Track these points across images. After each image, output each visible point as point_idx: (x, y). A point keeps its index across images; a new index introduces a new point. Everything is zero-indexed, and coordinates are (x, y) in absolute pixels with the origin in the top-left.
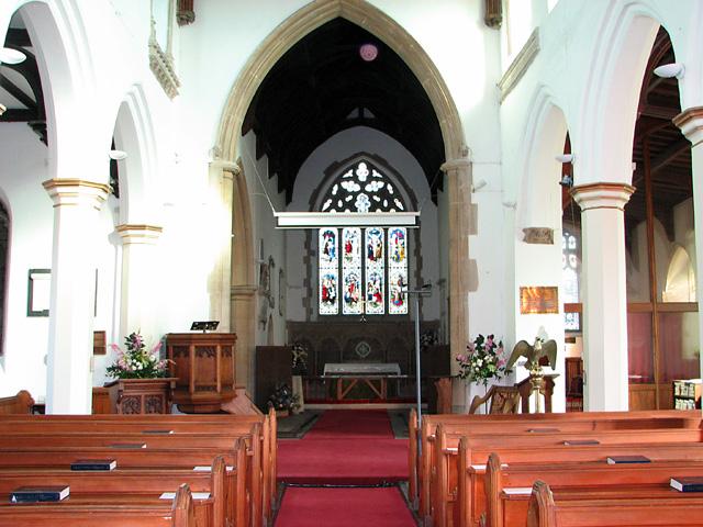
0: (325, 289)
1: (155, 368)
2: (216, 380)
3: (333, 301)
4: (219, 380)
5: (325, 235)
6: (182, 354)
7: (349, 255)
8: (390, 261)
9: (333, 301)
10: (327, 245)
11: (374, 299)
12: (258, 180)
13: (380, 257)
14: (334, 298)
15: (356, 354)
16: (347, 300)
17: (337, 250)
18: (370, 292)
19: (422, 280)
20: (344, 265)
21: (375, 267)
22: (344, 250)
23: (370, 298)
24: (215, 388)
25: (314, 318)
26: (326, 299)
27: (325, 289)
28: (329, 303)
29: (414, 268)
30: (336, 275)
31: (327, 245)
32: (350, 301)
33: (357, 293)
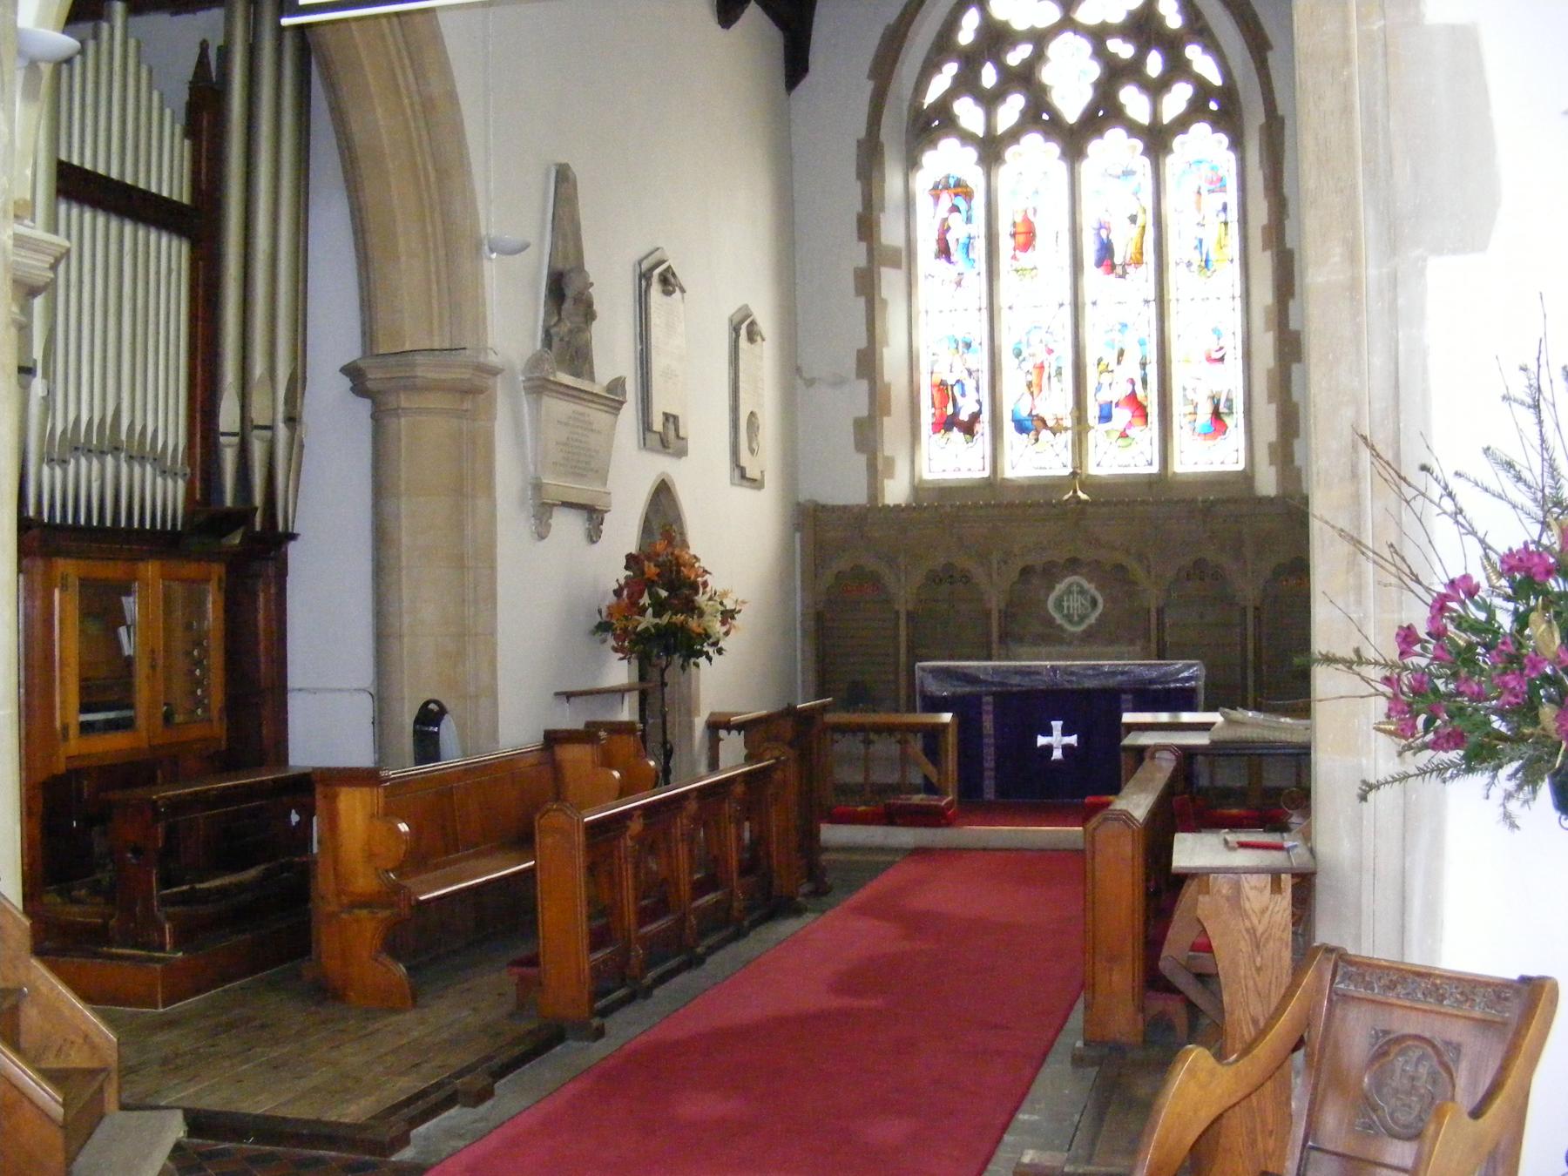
3: (969, 429)
5: (936, 191)
7: (1026, 259)
8: (1174, 275)
9: (969, 429)
10: (944, 230)
11: (1122, 416)
13: (1138, 262)
14: (975, 417)
15: (1050, 622)
16: (1021, 427)
17: (980, 246)
18: (1106, 396)
20: (1003, 299)
21: (1118, 305)
22: (1006, 244)
23: (1106, 417)
25: (896, 492)
26: (946, 423)
28: (956, 435)
29: (1264, 295)
30: (980, 333)
31: (944, 230)
33: (1056, 403)
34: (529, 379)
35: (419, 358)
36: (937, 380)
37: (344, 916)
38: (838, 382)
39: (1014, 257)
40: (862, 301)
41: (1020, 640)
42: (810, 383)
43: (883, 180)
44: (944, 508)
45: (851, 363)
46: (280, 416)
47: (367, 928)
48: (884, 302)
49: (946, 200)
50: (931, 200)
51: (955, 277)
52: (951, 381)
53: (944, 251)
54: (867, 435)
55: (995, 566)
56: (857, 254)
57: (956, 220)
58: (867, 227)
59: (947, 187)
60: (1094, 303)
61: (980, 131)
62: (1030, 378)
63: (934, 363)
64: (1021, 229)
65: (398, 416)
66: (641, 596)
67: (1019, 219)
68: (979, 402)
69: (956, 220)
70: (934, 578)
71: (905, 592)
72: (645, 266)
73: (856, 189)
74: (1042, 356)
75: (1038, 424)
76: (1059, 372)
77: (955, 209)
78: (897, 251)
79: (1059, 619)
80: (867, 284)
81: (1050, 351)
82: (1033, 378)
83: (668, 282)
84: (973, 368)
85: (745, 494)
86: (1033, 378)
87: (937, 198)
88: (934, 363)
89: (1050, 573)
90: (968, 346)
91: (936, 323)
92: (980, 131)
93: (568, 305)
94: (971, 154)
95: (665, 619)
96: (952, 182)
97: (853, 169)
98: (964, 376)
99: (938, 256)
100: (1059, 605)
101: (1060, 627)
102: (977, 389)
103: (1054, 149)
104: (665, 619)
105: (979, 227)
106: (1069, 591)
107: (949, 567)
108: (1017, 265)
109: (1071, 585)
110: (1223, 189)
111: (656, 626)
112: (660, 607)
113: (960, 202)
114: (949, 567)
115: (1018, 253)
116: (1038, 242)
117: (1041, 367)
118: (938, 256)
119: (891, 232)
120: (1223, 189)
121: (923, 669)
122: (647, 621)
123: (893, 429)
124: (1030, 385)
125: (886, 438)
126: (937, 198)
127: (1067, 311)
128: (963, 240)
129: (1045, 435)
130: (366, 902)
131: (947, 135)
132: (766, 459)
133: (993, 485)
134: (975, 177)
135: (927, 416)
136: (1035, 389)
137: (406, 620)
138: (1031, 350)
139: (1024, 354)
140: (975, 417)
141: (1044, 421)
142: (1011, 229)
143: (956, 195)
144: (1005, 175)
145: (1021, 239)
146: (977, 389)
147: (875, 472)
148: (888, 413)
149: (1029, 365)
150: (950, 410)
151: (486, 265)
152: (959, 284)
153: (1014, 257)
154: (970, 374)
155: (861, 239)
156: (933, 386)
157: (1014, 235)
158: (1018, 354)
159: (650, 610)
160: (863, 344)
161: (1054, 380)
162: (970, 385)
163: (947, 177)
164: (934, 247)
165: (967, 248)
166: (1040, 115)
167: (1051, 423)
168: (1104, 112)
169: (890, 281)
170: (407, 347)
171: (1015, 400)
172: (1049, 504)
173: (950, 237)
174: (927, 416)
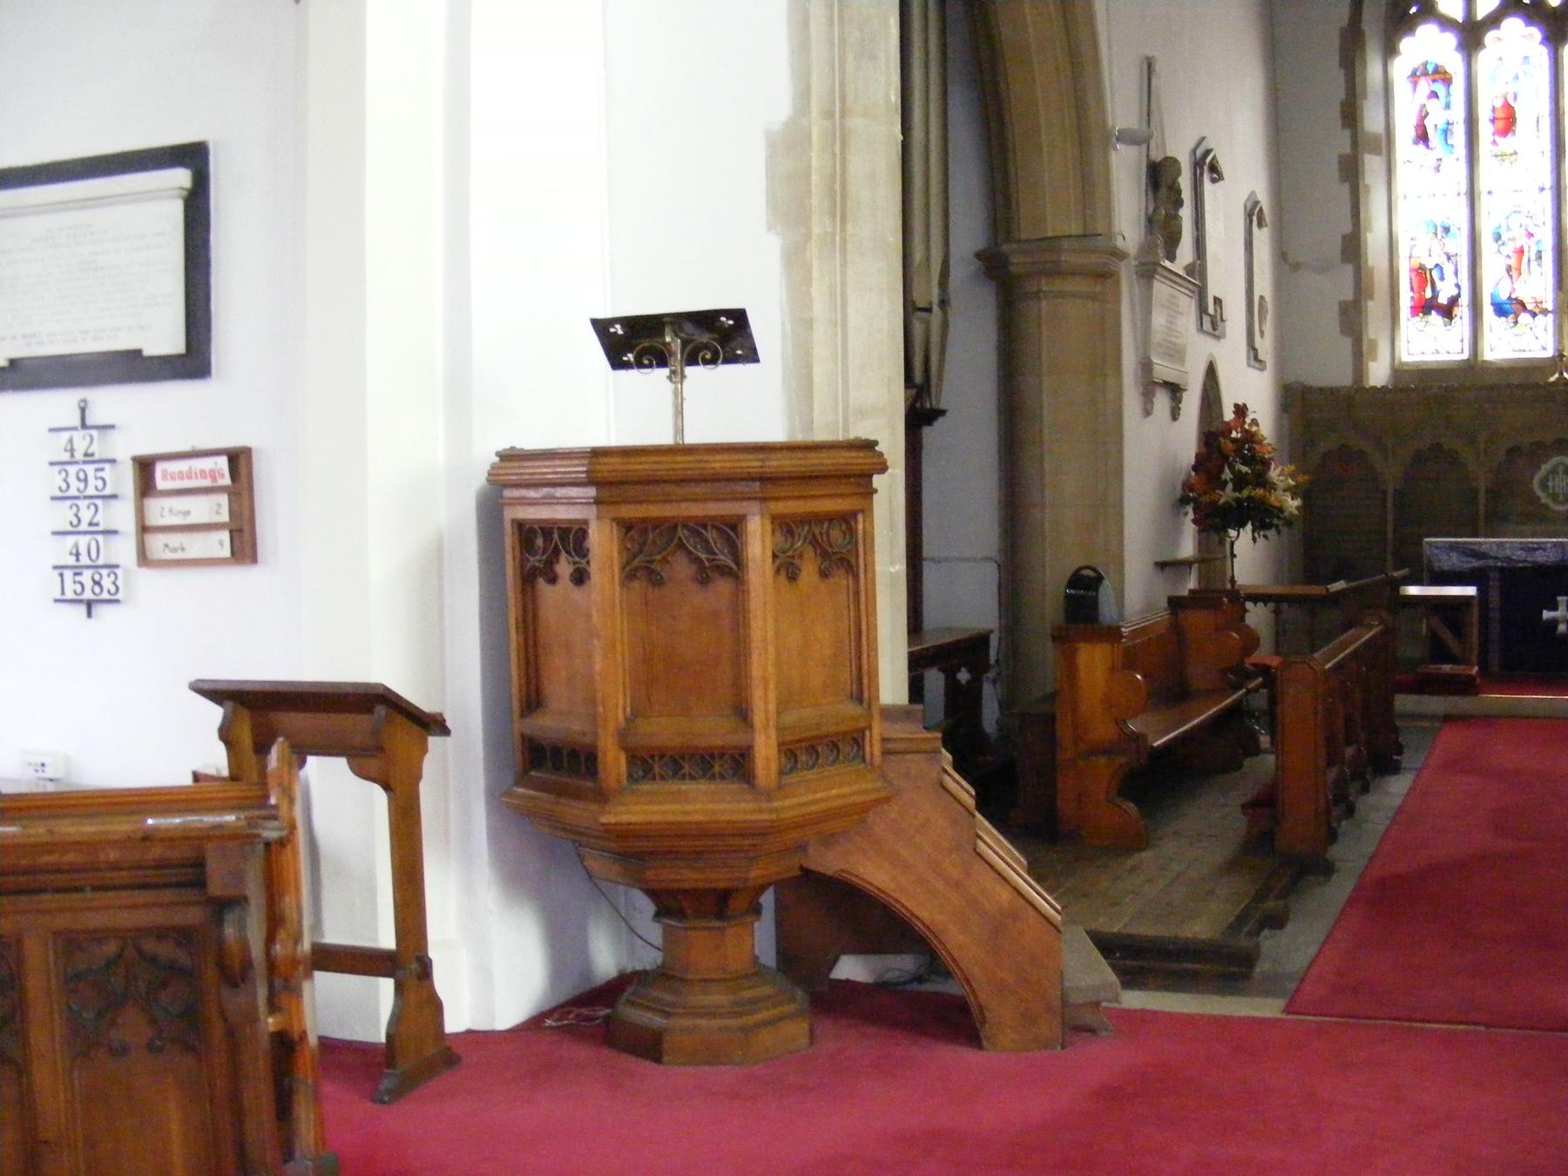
0: (1422, 275)
1: (1291, 482)
2: (742, 713)
3: (1447, 312)
4: (763, 705)
5: (1414, 77)
6: (564, 568)
7: (1507, 144)
9: (1447, 312)
10: (1423, 116)
12: (839, 111)
14: (1454, 301)
15: (1535, 500)
16: (1500, 310)
17: (1459, 132)
19: (436, 1006)
20: (1483, 184)
22: (1485, 129)
24: (739, 763)
25: (1378, 374)
26: (1424, 307)
27: (1421, 274)
28: (1435, 317)
31: (1423, 116)
32: (1509, 309)
34: (1142, 264)
35: (1066, 244)
36: (1415, 264)
37: (1081, 763)
38: (1324, 268)
39: (1494, 142)
40: (1347, 186)
41: (1505, 519)
42: (1296, 267)
43: (1365, 68)
44: (1429, 390)
45: (1334, 247)
46: (935, 300)
47: (1104, 771)
48: (1368, 187)
49: (1424, 86)
50: (1409, 87)
51: (1434, 163)
52: (1429, 265)
53: (1422, 137)
54: (1351, 318)
55: (1482, 446)
57: (1434, 107)
58: (1350, 114)
59: (1425, 74)
60: (1542, 189)
61: (1458, 14)
62: (1510, 262)
63: (1413, 247)
64: (1500, 115)
65: (1039, 299)
66: (1222, 471)
67: (1499, 104)
68: (1458, 286)
69: (1434, 107)
70: (1419, 458)
71: (1391, 472)
72: (1199, 152)
73: (1339, 77)
74: (1522, 241)
75: (1517, 307)
76: (1539, 256)
77: (1434, 95)
78: (1377, 138)
79: (1544, 499)
80: (1351, 171)
81: (1530, 235)
82: (1512, 262)
83: (1214, 168)
84: (1452, 251)
85: (1253, 374)
86: (1512, 262)
87: (1415, 84)
88: (1413, 247)
89: (1538, 452)
90: (1447, 230)
91: (1415, 207)
92: (1458, 14)
93: (1163, 192)
94: (1451, 39)
95: (1245, 493)
96: (1430, 68)
97: (1337, 59)
98: (1442, 260)
99: (1416, 143)
100: (1544, 485)
101: (1546, 507)
102: (1456, 273)
103: (1535, 33)
104: (1245, 493)
105: (1458, 114)
106: (1554, 471)
107: (1437, 447)
108: (1496, 150)
109: (1557, 466)
111: (1238, 500)
112: (1240, 482)
113: (1439, 88)
114: (1437, 447)
115: (1497, 138)
116: (1519, 126)
117: (1521, 252)
118: (1416, 143)
119: (1372, 121)
121: (1430, 544)
122: (1228, 495)
123: (1375, 309)
124: (1509, 269)
125: (1370, 321)
126: (1415, 84)
127: (1547, 197)
128: (1442, 126)
129: (1524, 318)
130: (1106, 750)
131: (1426, 21)
132: (1265, 346)
133: (1473, 367)
134: (1454, 63)
135: (1406, 299)
136: (1514, 273)
137: (1048, 492)
138: (1510, 235)
139: (1504, 238)
140: (1454, 301)
141: (1522, 304)
142: (1490, 115)
143: (1434, 81)
144: (1484, 60)
145: (1500, 124)
146: (1456, 273)
147: (1359, 357)
148: (1372, 298)
149: (1509, 249)
150: (1428, 294)
151: (1114, 158)
152: (1437, 169)
153: (1494, 142)
154: (1449, 258)
155: (1344, 126)
156: (1412, 270)
157: (1493, 120)
158: (1498, 237)
159: (1230, 486)
160: (1347, 228)
161: (1534, 264)
162: (1448, 269)
163: (1425, 64)
164: (1412, 133)
165: (1446, 133)
167: (1529, 307)
169: (1372, 165)
170: (1050, 234)
171: (1495, 283)
172: (1537, 386)
173: (1429, 123)
174: (1406, 299)
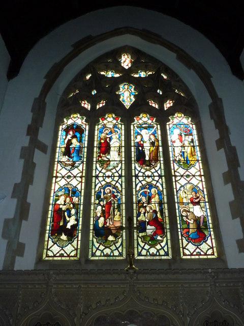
9: (71, 234)
11: (150, 229)
14: (74, 227)
21: (151, 176)
26: (58, 230)
56: (26, 141)
57: (74, 141)
69: (74, 141)
73: (19, 165)
110: (191, 134)
119: (43, 136)
120: (191, 134)
145: (103, 149)
153: (100, 156)
166: (115, 106)
168: (139, 107)
